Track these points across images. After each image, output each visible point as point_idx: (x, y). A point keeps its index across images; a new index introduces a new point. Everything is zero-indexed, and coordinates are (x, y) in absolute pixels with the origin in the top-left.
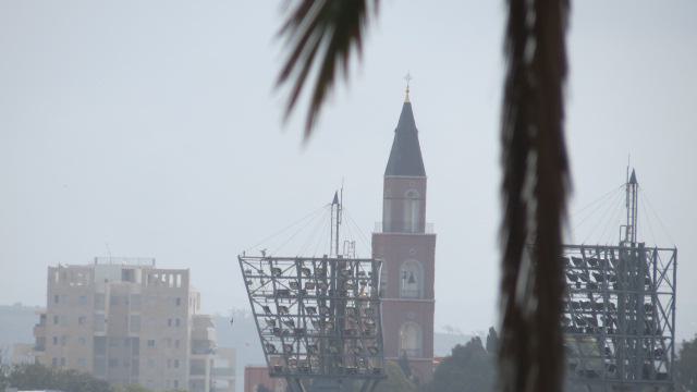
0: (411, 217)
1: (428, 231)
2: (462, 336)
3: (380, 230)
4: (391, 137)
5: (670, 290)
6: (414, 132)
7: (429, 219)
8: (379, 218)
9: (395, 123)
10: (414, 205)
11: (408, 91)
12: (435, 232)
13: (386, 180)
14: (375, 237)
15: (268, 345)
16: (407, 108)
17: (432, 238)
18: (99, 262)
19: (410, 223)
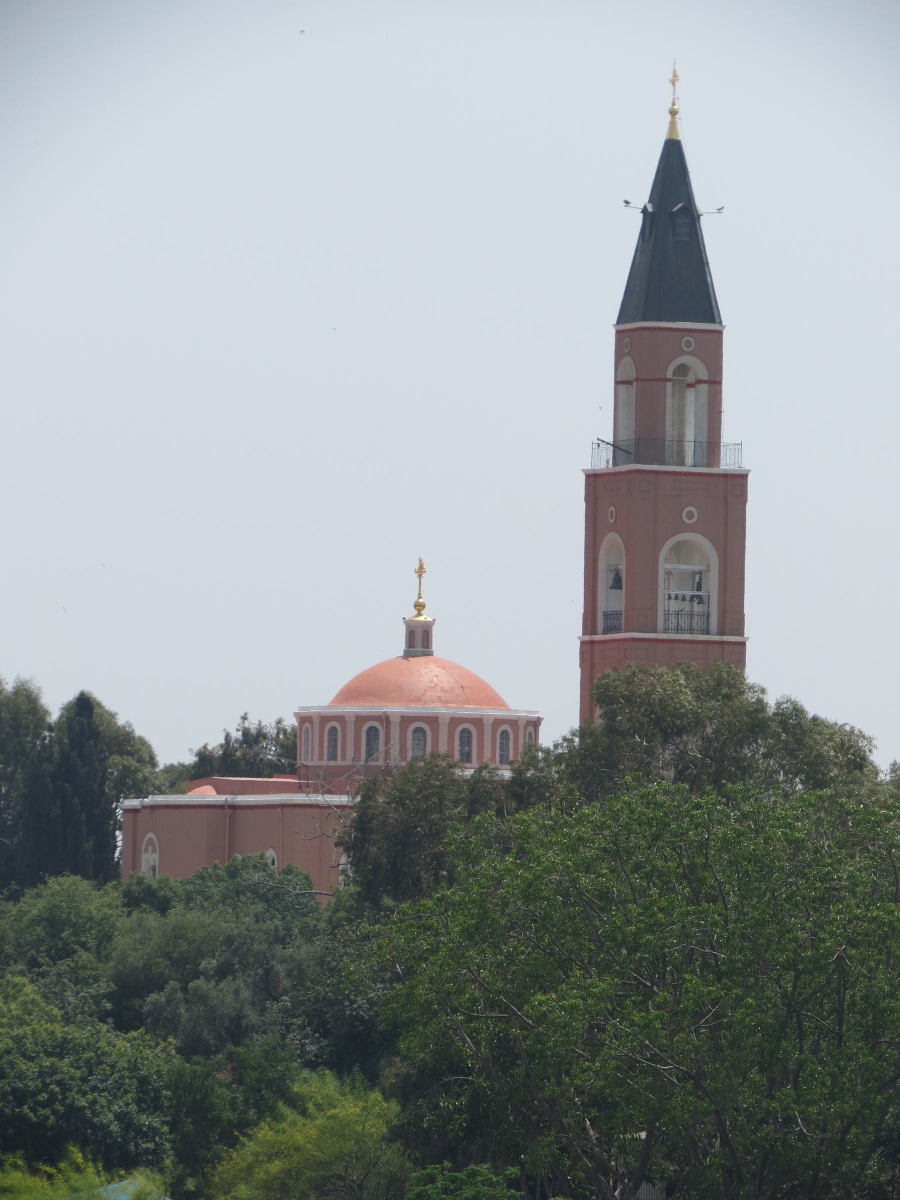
0: (681, 423)
1: (727, 463)
2: (503, 780)
3: (603, 461)
4: (632, 226)
5: (279, 810)
6: (691, 216)
7: (728, 434)
8: (605, 428)
9: (641, 193)
10: (694, 402)
11: (673, 113)
12: (746, 465)
13: (620, 334)
14: (593, 479)
15: (130, 753)
16: (673, 160)
17: (740, 479)
18: (632, 375)
19: (681, 441)
